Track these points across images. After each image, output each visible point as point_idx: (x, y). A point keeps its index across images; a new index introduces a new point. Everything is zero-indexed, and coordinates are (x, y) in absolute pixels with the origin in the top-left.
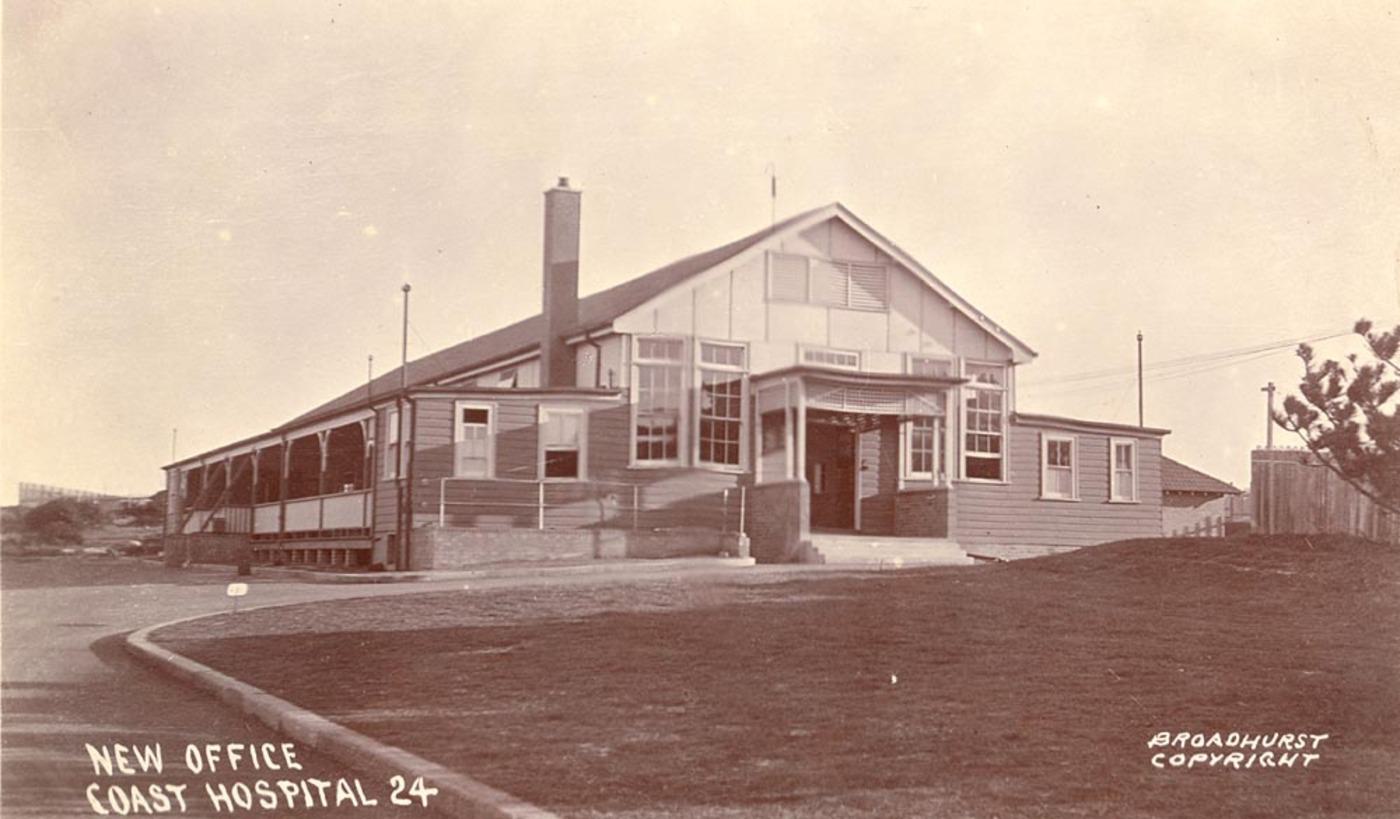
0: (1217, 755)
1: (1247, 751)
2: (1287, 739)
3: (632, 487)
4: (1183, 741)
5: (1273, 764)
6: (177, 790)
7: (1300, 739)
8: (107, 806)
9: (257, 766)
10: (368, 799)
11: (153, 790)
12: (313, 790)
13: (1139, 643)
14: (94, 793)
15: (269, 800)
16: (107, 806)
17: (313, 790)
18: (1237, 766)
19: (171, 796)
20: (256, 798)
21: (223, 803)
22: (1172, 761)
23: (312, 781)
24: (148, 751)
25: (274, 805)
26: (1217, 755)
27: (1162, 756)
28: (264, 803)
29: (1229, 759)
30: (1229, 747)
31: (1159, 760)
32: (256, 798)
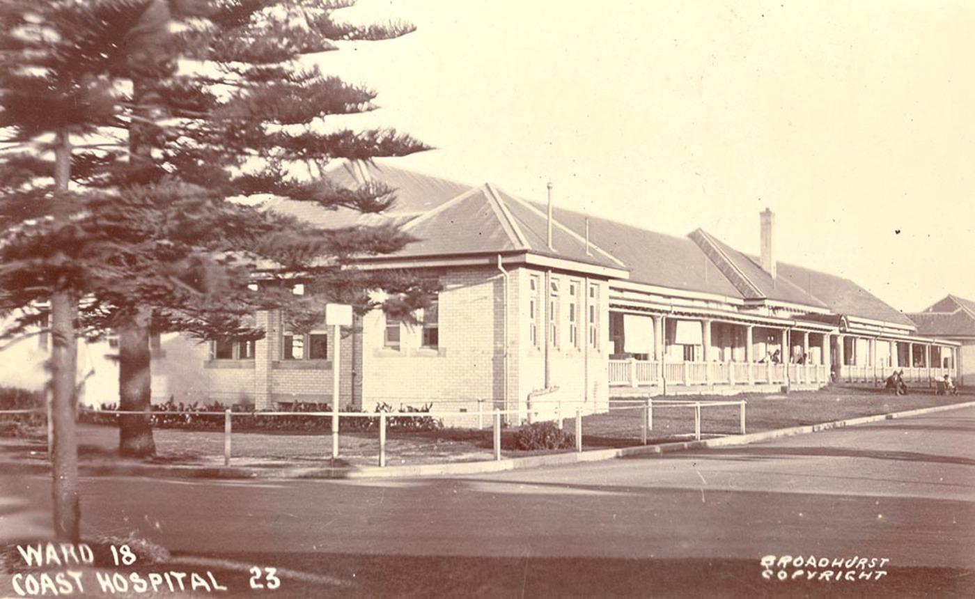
0: (812, 572)
1: (836, 569)
2: (863, 562)
3: (340, 453)
4: (863, 563)
5: (853, 579)
6: (77, 576)
7: (873, 561)
8: (25, 590)
9: (209, 574)
10: (219, 584)
11: (59, 578)
12: (174, 580)
13: (765, 508)
14: (17, 579)
15: (141, 585)
16: (25, 590)
17: (174, 580)
18: (828, 579)
19: (72, 581)
20: (131, 585)
21: (108, 589)
22: (782, 572)
23: (173, 573)
24: (30, 549)
25: (144, 589)
26: (812, 572)
27: (853, 572)
28: (137, 588)
29: (822, 575)
30: (821, 567)
31: (851, 575)
32: (131, 585)
